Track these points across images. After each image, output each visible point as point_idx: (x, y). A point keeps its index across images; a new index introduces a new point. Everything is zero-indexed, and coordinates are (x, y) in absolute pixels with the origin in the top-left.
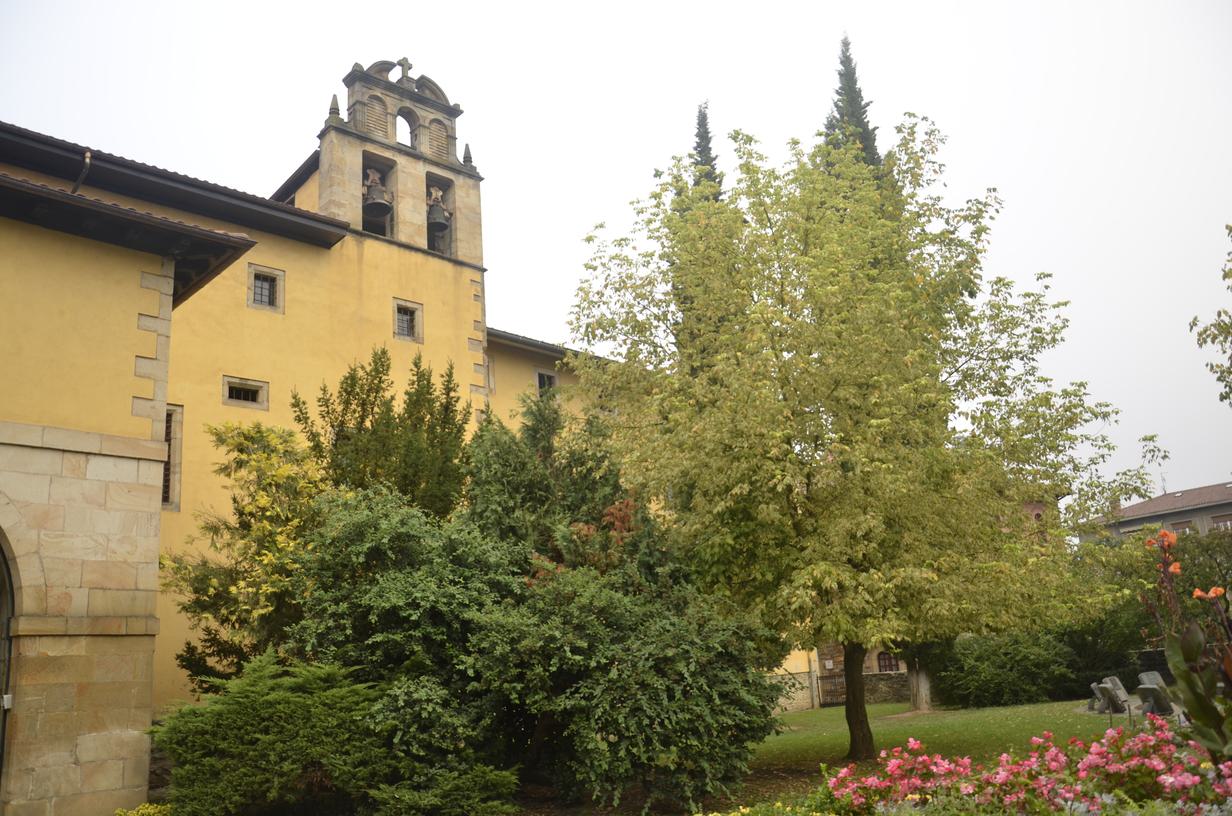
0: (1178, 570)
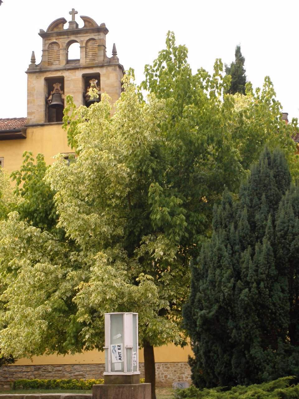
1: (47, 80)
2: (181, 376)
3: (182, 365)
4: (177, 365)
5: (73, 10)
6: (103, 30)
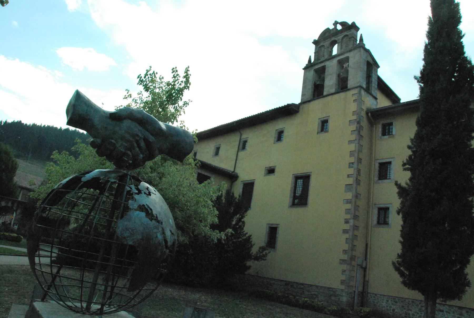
1: (316, 71)
2: (407, 312)
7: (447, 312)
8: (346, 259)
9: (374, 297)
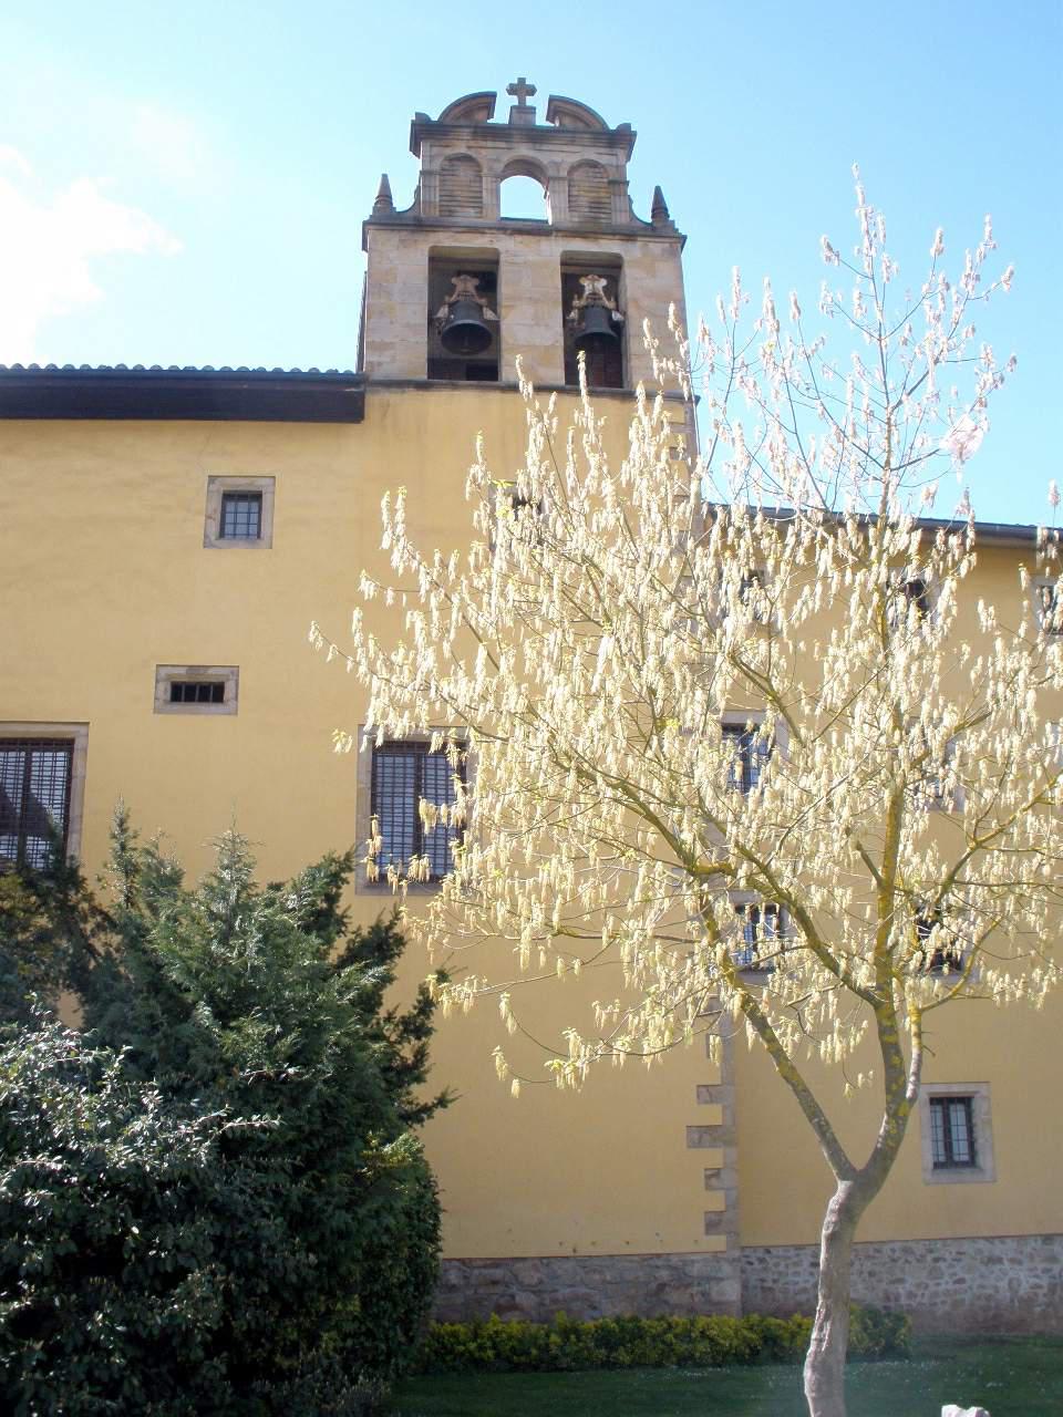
0: (199, 1380)
2: (892, 1289)
3: (893, 1251)
4: (878, 1251)
5: (522, 81)
6: (622, 139)
7: (1012, 1261)
8: (719, 1122)
9: (761, 1260)
